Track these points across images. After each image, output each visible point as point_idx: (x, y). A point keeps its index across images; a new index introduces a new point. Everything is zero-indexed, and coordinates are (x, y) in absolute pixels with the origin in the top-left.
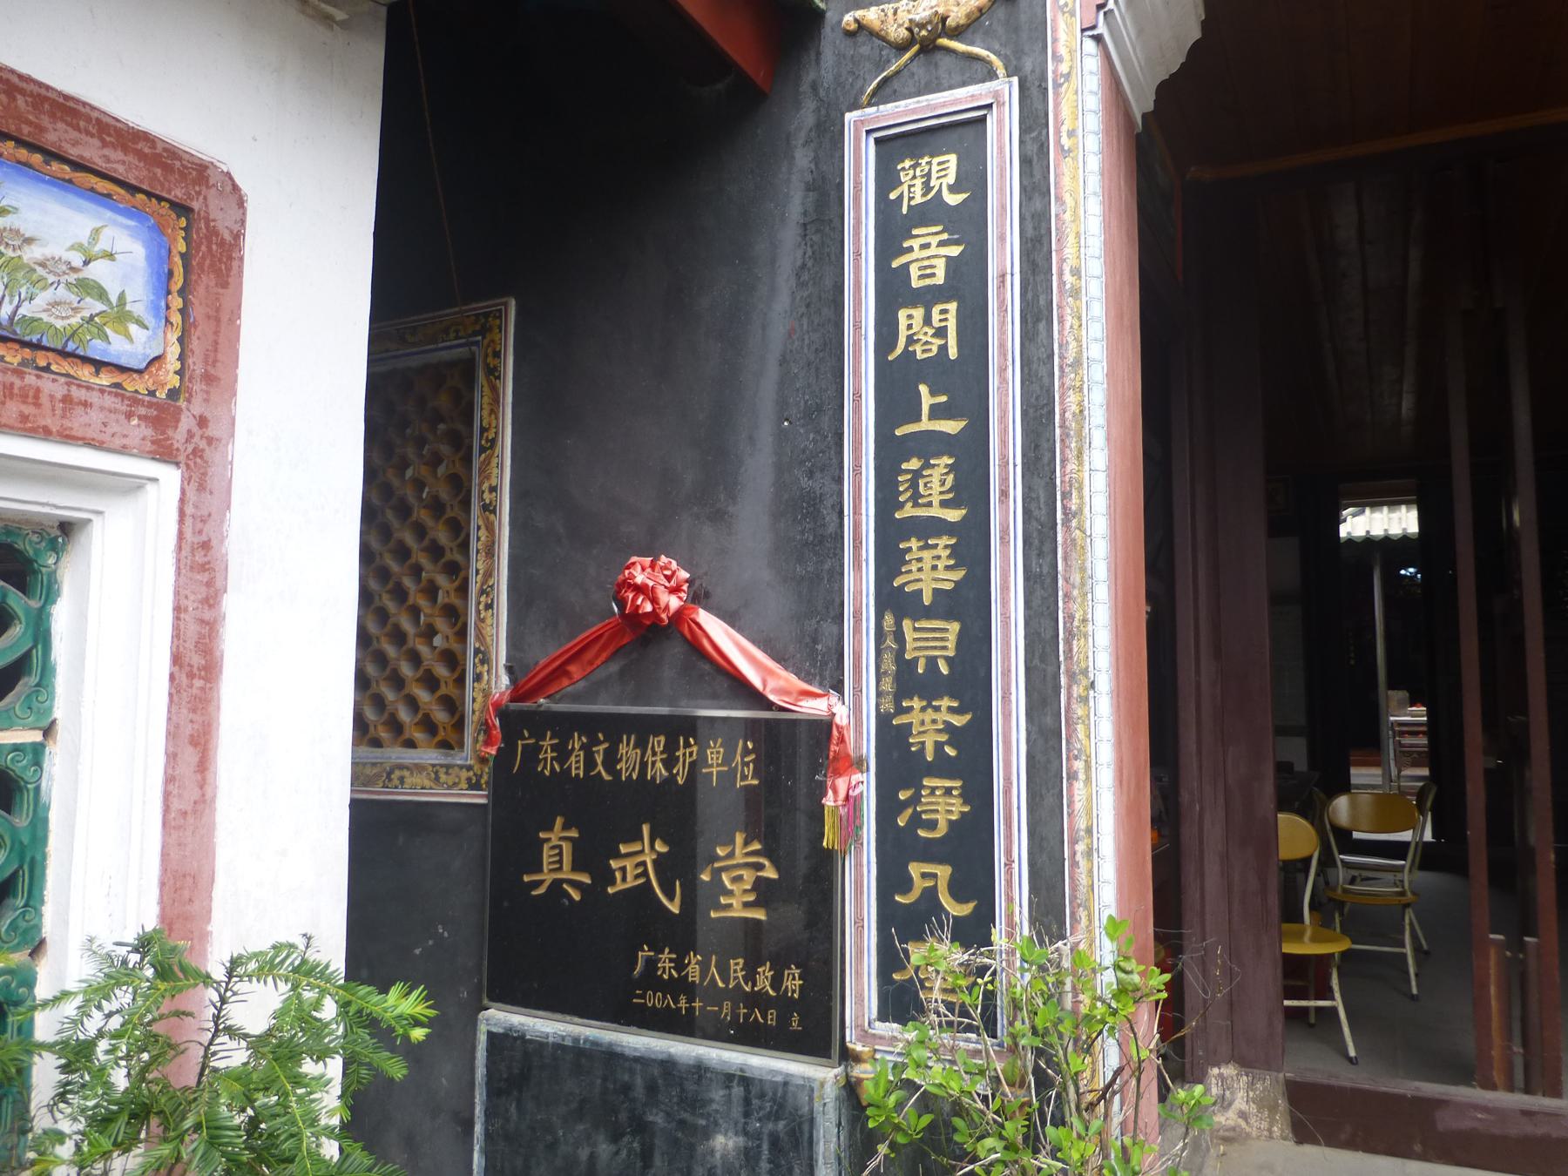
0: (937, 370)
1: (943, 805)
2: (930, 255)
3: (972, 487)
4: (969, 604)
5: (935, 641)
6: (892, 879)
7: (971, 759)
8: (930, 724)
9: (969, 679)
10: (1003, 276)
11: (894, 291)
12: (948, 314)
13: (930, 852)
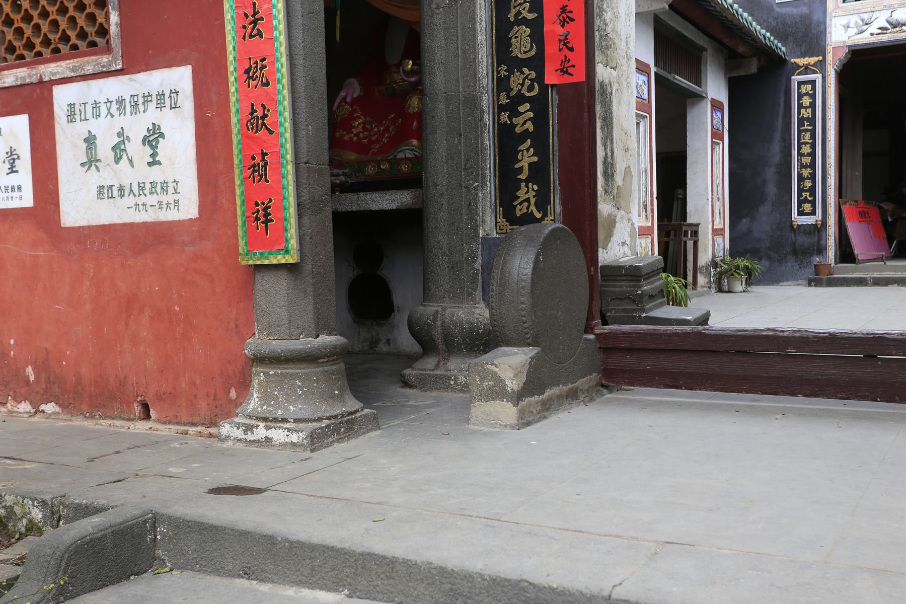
0: (808, 119)
1: (808, 184)
2: (806, 101)
3: (813, 137)
4: (813, 154)
5: (807, 160)
6: (800, 195)
7: (813, 177)
8: (806, 172)
9: (813, 165)
10: (646, 206)
11: (800, 106)
12: (809, 110)
13: (806, 191)
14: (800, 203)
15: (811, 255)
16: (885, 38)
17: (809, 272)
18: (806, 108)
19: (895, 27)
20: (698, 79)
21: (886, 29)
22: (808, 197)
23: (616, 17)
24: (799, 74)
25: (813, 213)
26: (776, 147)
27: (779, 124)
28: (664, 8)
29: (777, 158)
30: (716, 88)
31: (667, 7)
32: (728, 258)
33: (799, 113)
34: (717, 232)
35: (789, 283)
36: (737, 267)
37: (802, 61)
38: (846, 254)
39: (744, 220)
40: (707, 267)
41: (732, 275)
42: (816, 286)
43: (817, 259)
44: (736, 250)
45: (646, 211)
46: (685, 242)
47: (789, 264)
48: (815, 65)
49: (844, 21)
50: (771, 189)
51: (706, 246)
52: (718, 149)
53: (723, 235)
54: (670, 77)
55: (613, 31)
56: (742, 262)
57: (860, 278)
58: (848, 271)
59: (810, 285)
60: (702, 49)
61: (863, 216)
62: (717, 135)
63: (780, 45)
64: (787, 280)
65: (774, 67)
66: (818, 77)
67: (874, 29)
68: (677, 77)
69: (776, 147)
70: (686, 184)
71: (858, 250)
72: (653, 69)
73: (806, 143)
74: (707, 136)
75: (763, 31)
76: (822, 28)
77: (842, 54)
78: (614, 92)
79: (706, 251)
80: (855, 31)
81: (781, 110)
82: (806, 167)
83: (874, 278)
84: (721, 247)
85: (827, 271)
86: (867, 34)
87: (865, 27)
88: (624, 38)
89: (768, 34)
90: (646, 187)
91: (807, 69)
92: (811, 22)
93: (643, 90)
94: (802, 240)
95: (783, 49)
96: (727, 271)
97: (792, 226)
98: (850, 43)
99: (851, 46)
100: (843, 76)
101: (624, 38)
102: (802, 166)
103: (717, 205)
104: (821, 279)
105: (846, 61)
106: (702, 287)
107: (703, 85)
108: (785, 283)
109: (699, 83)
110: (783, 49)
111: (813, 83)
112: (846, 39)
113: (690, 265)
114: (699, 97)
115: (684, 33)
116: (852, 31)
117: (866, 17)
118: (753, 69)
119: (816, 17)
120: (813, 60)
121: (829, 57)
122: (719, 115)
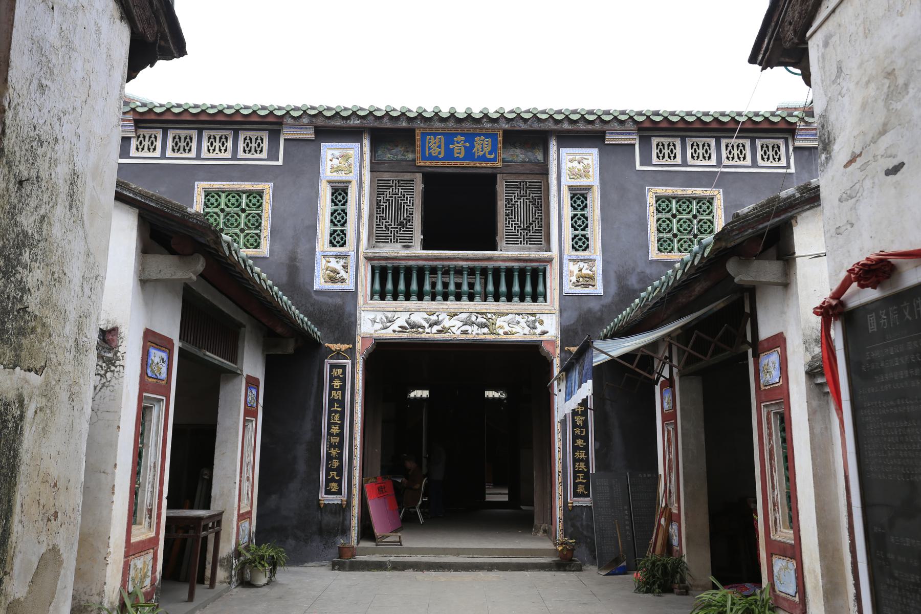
0: (337, 401)
1: (336, 464)
2: (337, 384)
3: (342, 418)
4: (341, 435)
7: (340, 457)
9: (340, 446)
11: (332, 388)
12: (339, 393)
13: (333, 470)
14: (328, 482)
15: (336, 535)
16: (405, 335)
17: (333, 552)
18: (337, 390)
19: (412, 328)
20: (234, 356)
21: (405, 328)
22: (335, 477)
23: (57, 280)
24: (331, 358)
25: (339, 492)
26: (308, 425)
27: (312, 403)
28: (190, 279)
29: (308, 436)
30: (252, 365)
31: (194, 278)
32: (253, 546)
33: (330, 394)
34: (242, 517)
35: (313, 564)
36: (262, 558)
37: (335, 347)
38: (367, 532)
39: (274, 497)
40: (229, 559)
41: (256, 566)
42: (339, 570)
43: (341, 541)
44: (263, 534)
45: (150, 518)
46: (205, 539)
47: (314, 544)
48: (346, 351)
49: (371, 315)
50: (301, 467)
51: (229, 535)
52: (251, 427)
53: (250, 518)
54: (199, 353)
55: (43, 303)
56: (267, 551)
57: (380, 562)
58: (368, 552)
59: (333, 569)
60: (240, 326)
61: (381, 491)
62: (250, 412)
63: (316, 329)
64: (312, 561)
65: (310, 349)
66: (348, 363)
67: (395, 326)
68: (208, 353)
69: (308, 425)
70: (213, 464)
71: (378, 531)
72: (177, 344)
73: (335, 424)
74: (239, 415)
75: (302, 316)
76: (353, 319)
77: (369, 344)
78: (29, 413)
79: (229, 540)
80: (380, 326)
81: (314, 390)
82: (334, 446)
83: (393, 562)
84: (247, 532)
85: (350, 554)
86: (390, 330)
87: (389, 324)
88: (73, 316)
89: (306, 319)
90: (153, 487)
91: (338, 355)
92: (343, 313)
93: (159, 369)
94: (328, 519)
95: (319, 333)
96: (251, 562)
97: (319, 505)
98: (376, 336)
99: (375, 339)
100: (369, 363)
101: (73, 316)
102: (331, 446)
103: (246, 485)
104: (344, 563)
105: (371, 351)
106: (221, 582)
107: (239, 361)
108: (310, 564)
109: (234, 361)
110: (318, 333)
111: (344, 367)
112: (373, 332)
113: (209, 557)
114: (234, 374)
115: (221, 307)
116: (378, 326)
117: (389, 315)
118: (290, 350)
119: (348, 308)
120: (344, 347)
121: (359, 346)
122: (254, 392)
